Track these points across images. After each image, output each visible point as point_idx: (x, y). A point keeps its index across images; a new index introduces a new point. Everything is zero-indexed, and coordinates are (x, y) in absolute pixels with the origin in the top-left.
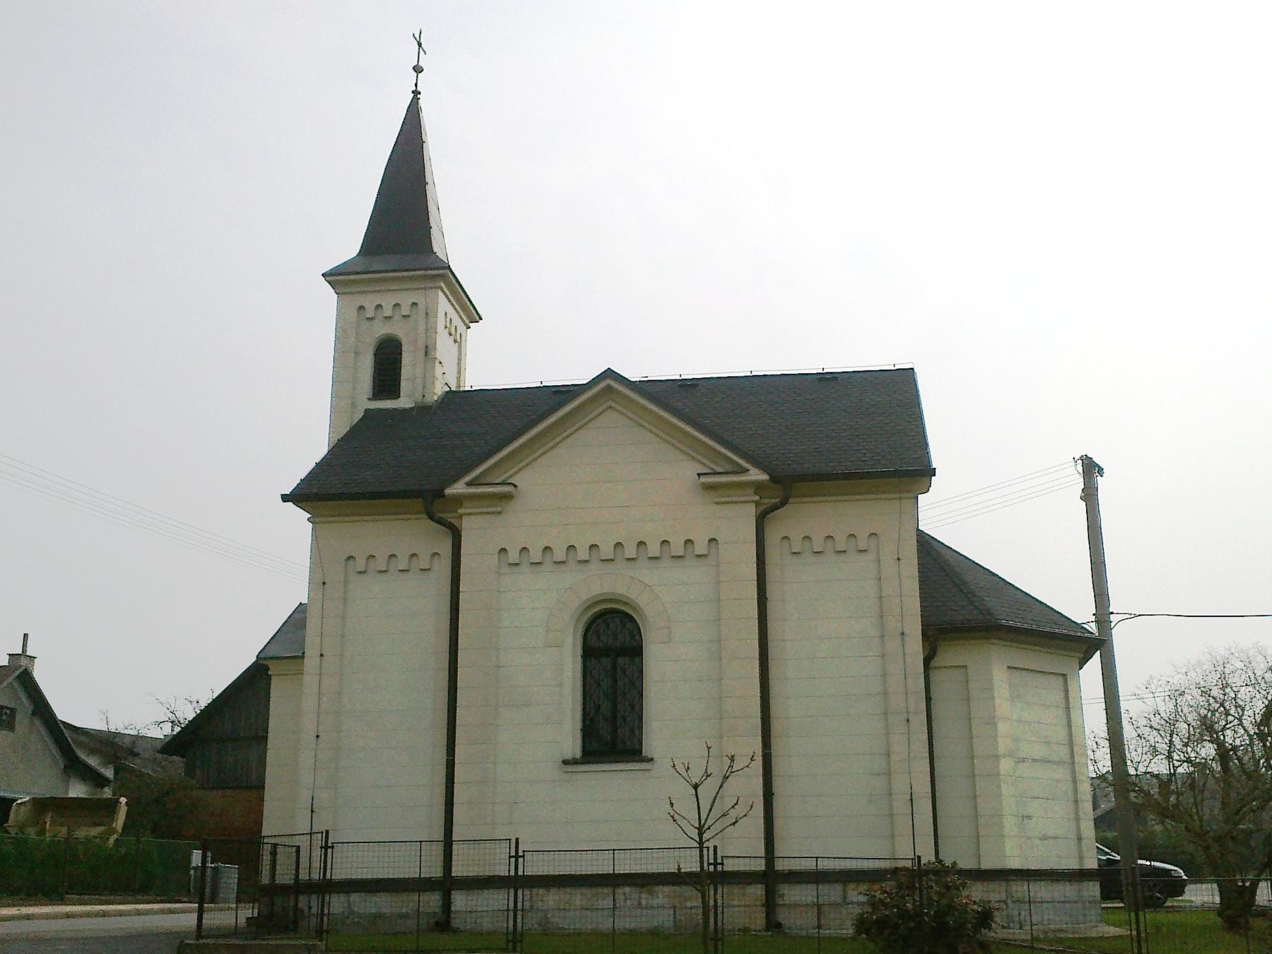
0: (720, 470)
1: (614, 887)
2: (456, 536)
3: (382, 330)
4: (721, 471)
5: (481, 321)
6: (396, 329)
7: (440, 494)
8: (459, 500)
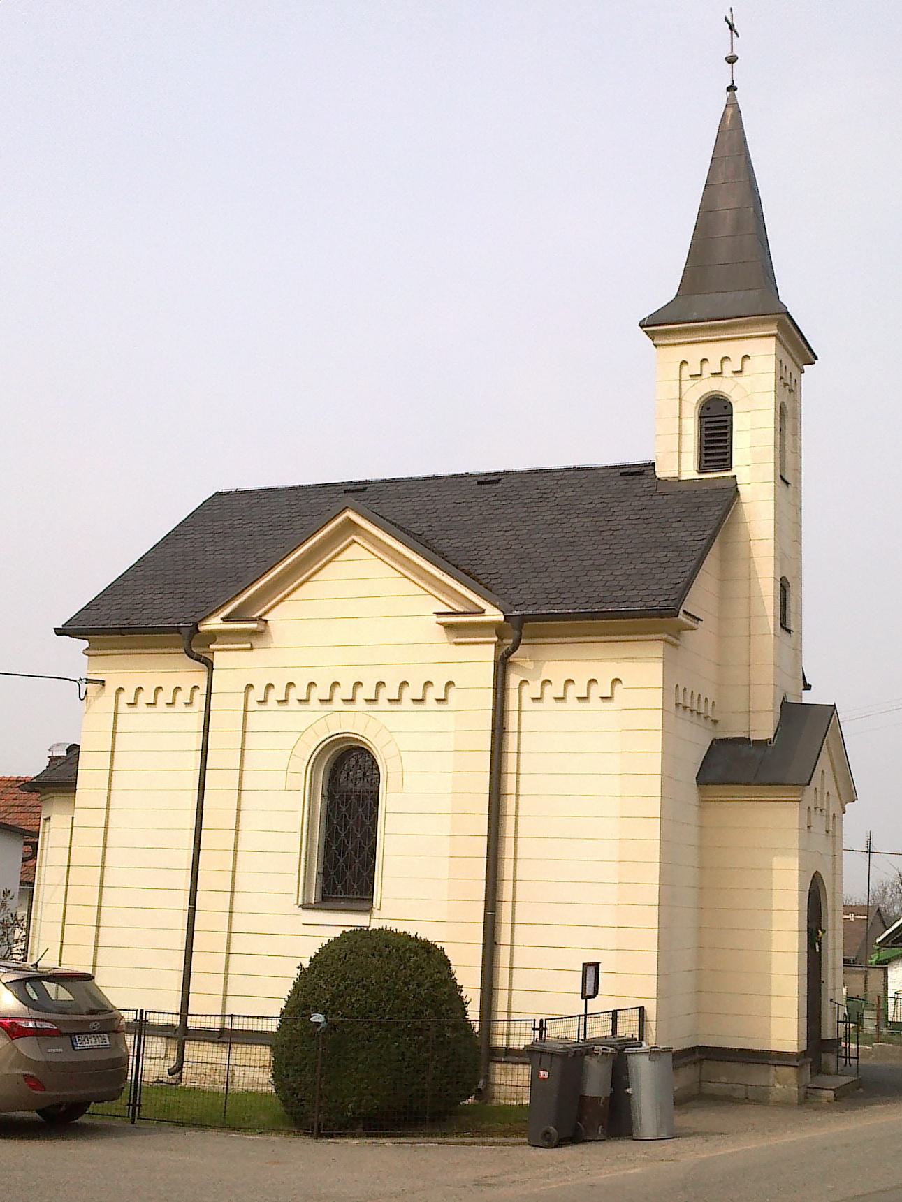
0: (460, 609)
1: (188, 1015)
2: (209, 665)
3: (709, 386)
4: (462, 610)
5: (816, 361)
6: (724, 386)
7: (195, 629)
8: (213, 636)
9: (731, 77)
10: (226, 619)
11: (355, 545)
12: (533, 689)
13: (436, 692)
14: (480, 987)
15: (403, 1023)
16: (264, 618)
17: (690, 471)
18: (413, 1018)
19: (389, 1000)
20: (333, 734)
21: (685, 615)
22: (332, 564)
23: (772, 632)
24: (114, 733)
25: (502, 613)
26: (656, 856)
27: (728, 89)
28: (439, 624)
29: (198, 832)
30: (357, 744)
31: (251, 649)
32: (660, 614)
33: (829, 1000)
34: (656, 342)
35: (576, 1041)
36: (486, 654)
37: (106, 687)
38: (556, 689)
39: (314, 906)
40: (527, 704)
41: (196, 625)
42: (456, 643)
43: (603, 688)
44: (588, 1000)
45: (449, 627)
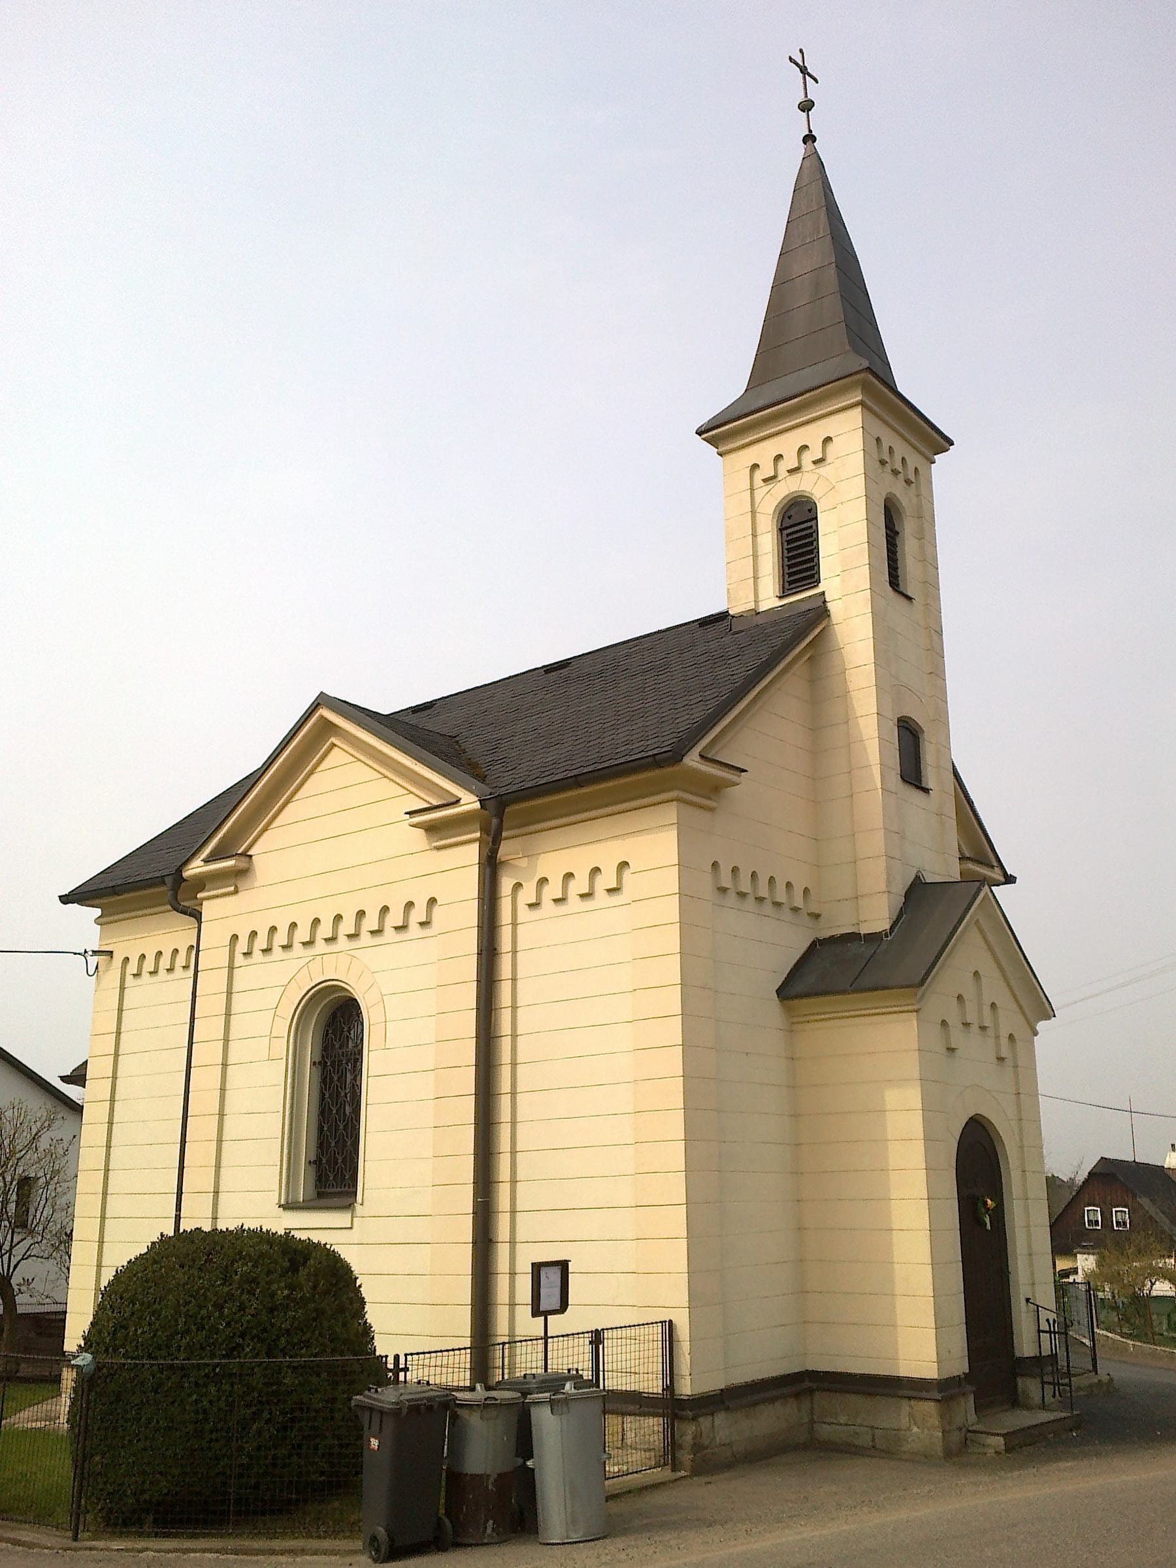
0: (435, 803)
2: (197, 916)
3: (787, 487)
8: (201, 883)
9: (807, 126)
10: (206, 861)
11: (336, 749)
12: (528, 894)
13: (418, 915)
14: (470, 1303)
15: (207, 1365)
16: (249, 853)
17: (769, 598)
18: (224, 1357)
19: (188, 1331)
20: (317, 982)
21: (703, 762)
22: (313, 777)
23: (879, 786)
24: (120, 1010)
25: (476, 799)
26: (677, 1100)
27: (805, 140)
28: (412, 826)
29: (185, 1119)
30: (343, 994)
31: (236, 892)
32: (656, 762)
33: (1023, 1302)
34: (722, 449)
35: (637, 1376)
36: (470, 854)
37: (114, 959)
38: (553, 889)
39: (301, 1205)
40: (524, 913)
41: (179, 871)
42: (438, 848)
43: (608, 879)
44: (549, 1317)
45: (432, 829)
